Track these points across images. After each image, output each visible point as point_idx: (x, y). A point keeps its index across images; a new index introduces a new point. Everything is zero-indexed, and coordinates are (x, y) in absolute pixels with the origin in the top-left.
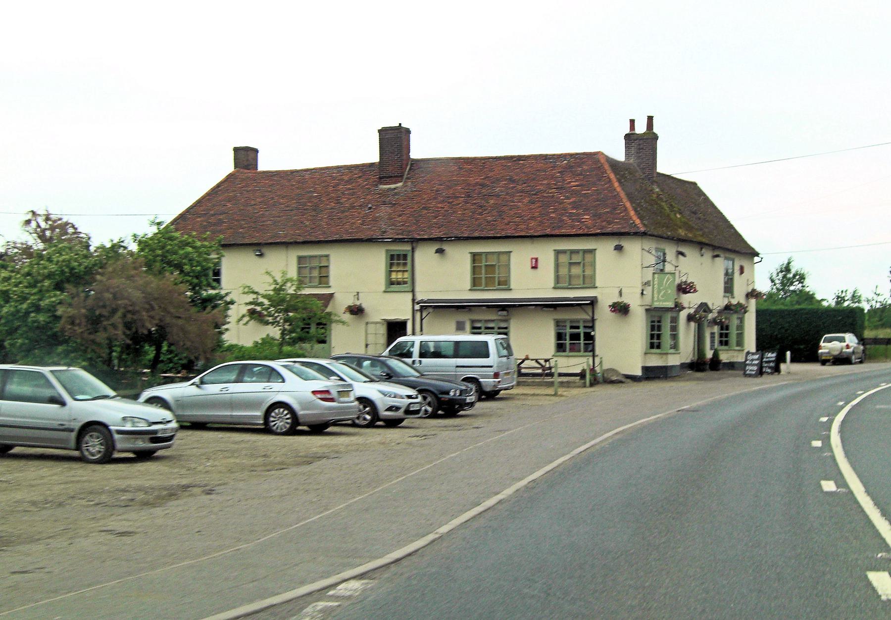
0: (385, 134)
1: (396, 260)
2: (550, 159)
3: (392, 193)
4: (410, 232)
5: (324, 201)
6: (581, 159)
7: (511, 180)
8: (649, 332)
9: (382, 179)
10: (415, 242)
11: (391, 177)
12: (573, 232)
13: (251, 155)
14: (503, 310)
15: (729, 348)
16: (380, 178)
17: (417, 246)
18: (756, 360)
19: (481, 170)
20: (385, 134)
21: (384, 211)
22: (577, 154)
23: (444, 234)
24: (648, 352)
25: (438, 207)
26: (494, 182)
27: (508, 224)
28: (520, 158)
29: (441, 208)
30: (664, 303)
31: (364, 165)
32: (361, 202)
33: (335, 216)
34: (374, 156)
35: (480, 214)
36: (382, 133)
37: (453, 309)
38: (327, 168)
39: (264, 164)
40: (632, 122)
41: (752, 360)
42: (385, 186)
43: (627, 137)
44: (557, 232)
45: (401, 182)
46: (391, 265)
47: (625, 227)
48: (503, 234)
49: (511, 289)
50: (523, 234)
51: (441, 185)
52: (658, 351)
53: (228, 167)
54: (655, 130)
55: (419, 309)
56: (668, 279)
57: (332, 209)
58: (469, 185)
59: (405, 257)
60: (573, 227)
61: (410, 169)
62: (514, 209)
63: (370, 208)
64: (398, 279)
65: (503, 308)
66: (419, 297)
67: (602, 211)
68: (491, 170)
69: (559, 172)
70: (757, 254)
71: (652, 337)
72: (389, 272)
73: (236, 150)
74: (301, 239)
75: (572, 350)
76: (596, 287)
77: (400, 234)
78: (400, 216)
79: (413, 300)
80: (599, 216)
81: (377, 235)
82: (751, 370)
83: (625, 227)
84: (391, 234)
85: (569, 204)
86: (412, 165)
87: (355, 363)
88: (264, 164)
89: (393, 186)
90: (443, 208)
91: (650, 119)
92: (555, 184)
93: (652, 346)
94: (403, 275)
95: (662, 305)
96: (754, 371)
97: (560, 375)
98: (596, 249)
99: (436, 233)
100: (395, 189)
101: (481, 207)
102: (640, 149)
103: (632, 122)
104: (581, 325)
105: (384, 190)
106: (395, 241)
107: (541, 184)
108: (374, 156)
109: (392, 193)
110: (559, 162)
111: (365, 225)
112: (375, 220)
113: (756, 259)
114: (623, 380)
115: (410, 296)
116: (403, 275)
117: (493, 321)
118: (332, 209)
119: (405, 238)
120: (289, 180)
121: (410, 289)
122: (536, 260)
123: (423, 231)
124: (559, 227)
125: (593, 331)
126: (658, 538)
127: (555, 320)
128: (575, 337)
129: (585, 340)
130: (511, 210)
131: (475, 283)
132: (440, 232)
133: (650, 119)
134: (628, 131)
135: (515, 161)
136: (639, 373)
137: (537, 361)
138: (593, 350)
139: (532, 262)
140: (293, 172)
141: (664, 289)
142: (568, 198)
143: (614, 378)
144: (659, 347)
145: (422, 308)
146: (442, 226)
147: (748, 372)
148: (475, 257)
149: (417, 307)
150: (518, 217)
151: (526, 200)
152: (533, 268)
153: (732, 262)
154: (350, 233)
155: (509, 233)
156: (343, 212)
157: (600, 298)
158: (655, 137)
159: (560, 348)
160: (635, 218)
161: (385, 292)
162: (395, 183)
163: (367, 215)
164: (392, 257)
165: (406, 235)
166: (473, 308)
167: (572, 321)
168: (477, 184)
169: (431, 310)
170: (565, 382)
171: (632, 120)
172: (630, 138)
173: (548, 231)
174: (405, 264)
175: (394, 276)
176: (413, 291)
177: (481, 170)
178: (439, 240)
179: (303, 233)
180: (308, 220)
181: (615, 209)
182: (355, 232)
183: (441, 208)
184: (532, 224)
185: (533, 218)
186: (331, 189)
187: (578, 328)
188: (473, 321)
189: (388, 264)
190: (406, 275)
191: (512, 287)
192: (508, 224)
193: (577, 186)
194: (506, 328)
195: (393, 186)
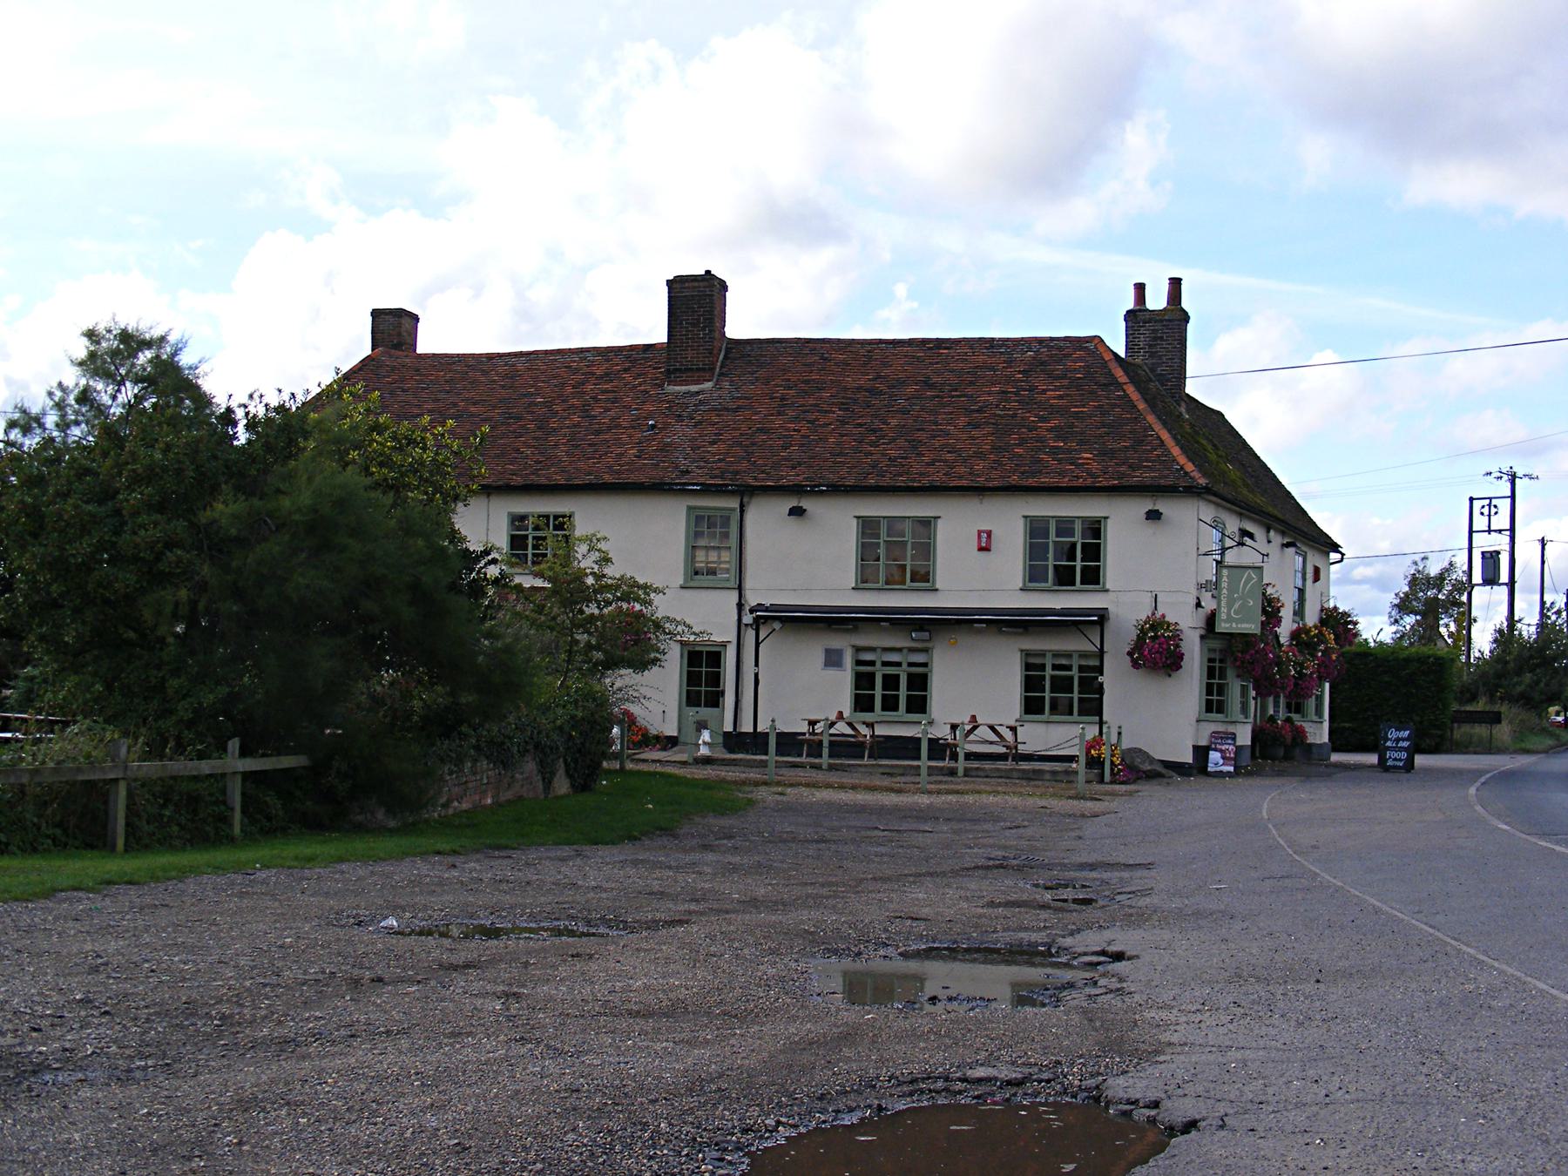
0: (678, 287)
1: (701, 525)
2: (1001, 346)
3: (693, 400)
4: (737, 473)
5: (557, 412)
6: (1060, 349)
7: (928, 384)
8: (1205, 680)
9: (673, 375)
10: (747, 492)
11: (691, 370)
12: (1065, 482)
13: (406, 322)
14: (921, 629)
15: (1227, 717)
16: (668, 372)
17: (748, 503)
18: (1403, 740)
19: (865, 365)
20: (678, 287)
21: (681, 433)
22: (1052, 339)
23: (806, 479)
24: (1202, 718)
25: (788, 430)
26: (894, 387)
27: (932, 463)
28: (940, 343)
29: (795, 430)
30: (1244, 626)
31: (632, 348)
32: (633, 415)
33: (583, 440)
34: (654, 330)
35: (874, 444)
36: (675, 286)
37: (821, 625)
38: (559, 351)
39: (429, 341)
40: (1140, 288)
41: (1398, 740)
42: (677, 388)
43: (1130, 315)
44: (1031, 482)
45: (709, 381)
46: (698, 535)
47: (1166, 477)
48: (925, 482)
49: (937, 590)
50: (964, 483)
51: (790, 388)
52: (1220, 716)
53: (356, 346)
54: (1185, 304)
55: (751, 621)
56: (1249, 579)
57: (575, 426)
58: (846, 389)
59: (726, 521)
60: (1062, 474)
61: (726, 357)
62: (939, 436)
63: (653, 427)
64: (708, 563)
65: (921, 625)
66: (752, 600)
67: (1116, 446)
68: (885, 364)
69: (1020, 372)
70: (1335, 547)
71: (1209, 691)
72: (692, 549)
73: (377, 314)
74: (518, 480)
75: (1054, 709)
76: (1107, 591)
77: (716, 477)
78: (713, 443)
79: (740, 606)
80: (1111, 454)
81: (672, 476)
82: (1395, 759)
83: (1166, 477)
84: (700, 475)
85: (1050, 430)
86: (728, 351)
87: (234, 745)
88: (429, 341)
89: (694, 388)
90: (799, 431)
91: (1176, 283)
92: (1016, 394)
93: (1209, 708)
94: (707, 556)
95: (1237, 628)
96: (1400, 760)
97: (970, 756)
98: (1106, 518)
99: (790, 477)
100: (698, 393)
101: (875, 431)
102: (1155, 339)
103: (1140, 288)
104: (1075, 663)
105: (676, 395)
106: (707, 490)
107: (989, 394)
108: (654, 330)
109: (693, 400)
110: (1018, 353)
111: (645, 459)
112: (665, 449)
113: (1334, 556)
114: (1164, 771)
115: (734, 596)
116: (707, 556)
117: (900, 650)
118: (575, 426)
119: (727, 485)
120: (485, 373)
121: (733, 583)
122: (989, 534)
123: (763, 472)
124: (1033, 474)
125: (1102, 675)
126: (242, 932)
127: (1022, 651)
128: (1062, 685)
129: (1080, 693)
130: (934, 437)
131: (865, 581)
132: (798, 475)
133: (1176, 283)
134: (1130, 305)
135: (930, 349)
136: (691, 761)
137: (992, 728)
138: (1100, 713)
139: (979, 537)
140: (491, 357)
141: (1240, 598)
142: (1043, 419)
143: (1147, 767)
144: (1220, 710)
145: (758, 623)
146: (800, 464)
147: (1390, 763)
148: (868, 526)
149: (748, 619)
150: (949, 452)
151: (962, 421)
152: (981, 549)
153: (1301, 559)
154: (619, 472)
155: (938, 478)
156: (598, 432)
157: (1112, 609)
158: (1185, 318)
159: (1032, 707)
160: (1182, 460)
161: (682, 587)
162: (698, 382)
163: (649, 439)
164: (699, 519)
165: (731, 479)
166: (860, 624)
167: (1056, 655)
168: (859, 389)
169: (777, 625)
170: (1048, 771)
171: (1140, 284)
172: (1137, 318)
173: (1014, 479)
174: (726, 536)
175: (700, 555)
176: (740, 588)
177: (865, 365)
178: (797, 490)
179: (520, 470)
180: (529, 447)
181: (1140, 442)
182: (627, 470)
183: (795, 430)
184: (980, 466)
185: (980, 455)
186: (569, 390)
187: (1069, 668)
188: (858, 649)
189: (692, 534)
190: (725, 556)
191: (938, 586)
192: (932, 463)
193: (1060, 397)
194: (925, 665)
195: (694, 388)
